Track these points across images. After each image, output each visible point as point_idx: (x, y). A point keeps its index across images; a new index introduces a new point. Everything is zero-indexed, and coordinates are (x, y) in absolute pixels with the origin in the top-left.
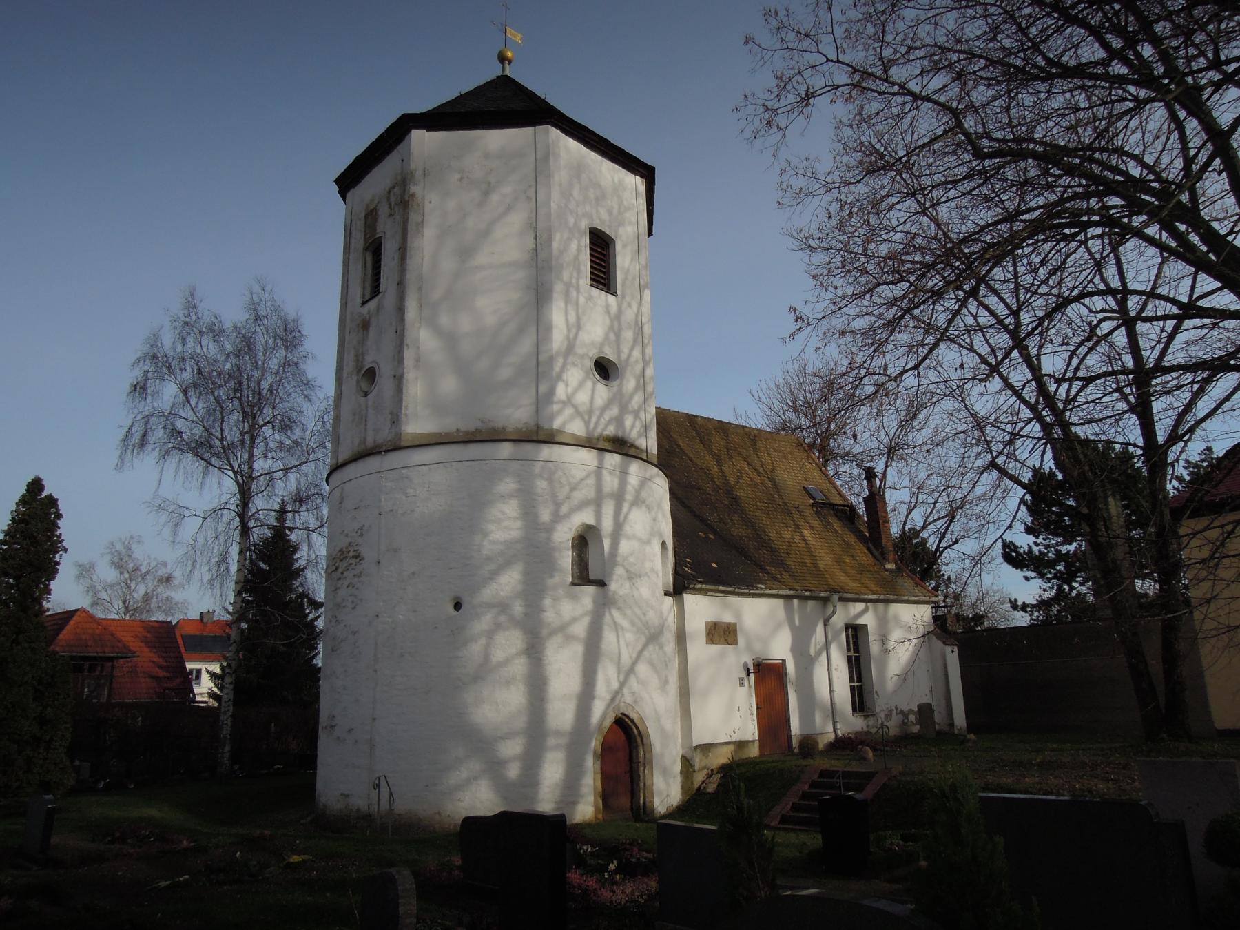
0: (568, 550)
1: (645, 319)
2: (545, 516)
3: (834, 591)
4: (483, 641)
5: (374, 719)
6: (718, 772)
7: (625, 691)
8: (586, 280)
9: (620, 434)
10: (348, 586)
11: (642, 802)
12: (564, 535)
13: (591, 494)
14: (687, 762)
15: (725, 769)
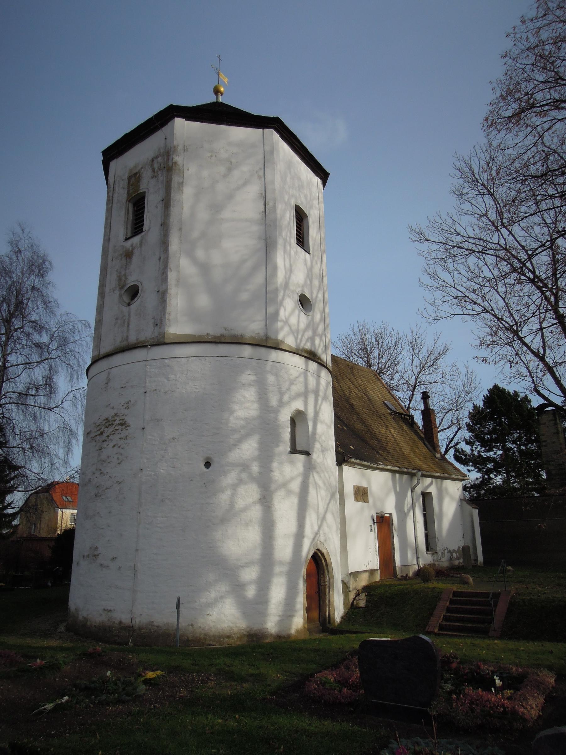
0: (288, 427)
1: (324, 274)
2: (274, 402)
3: (418, 469)
4: (229, 492)
5: (137, 550)
6: (362, 592)
7: (321, 532)
8: (294, 241)
9: (313, 350)
10: (114, 446)
11: (327, 614)
12: (285, 416)
13: (303, 389)
14: (345, 584)
15: (367, 589)
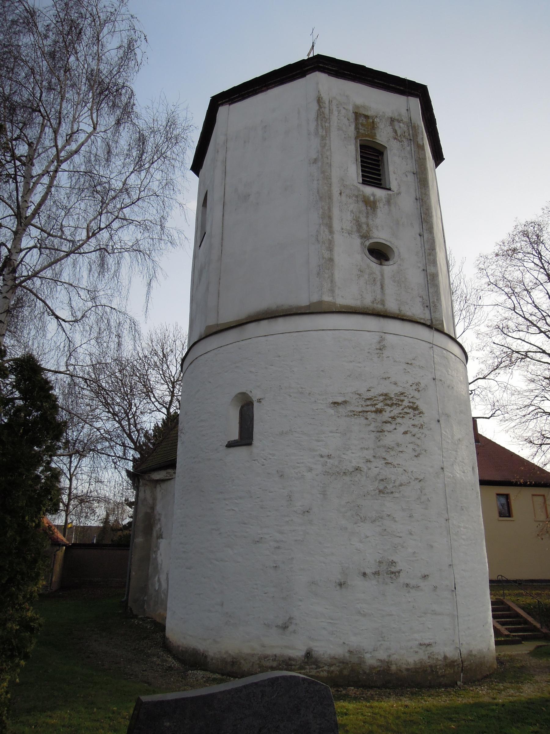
10: (405, 433)
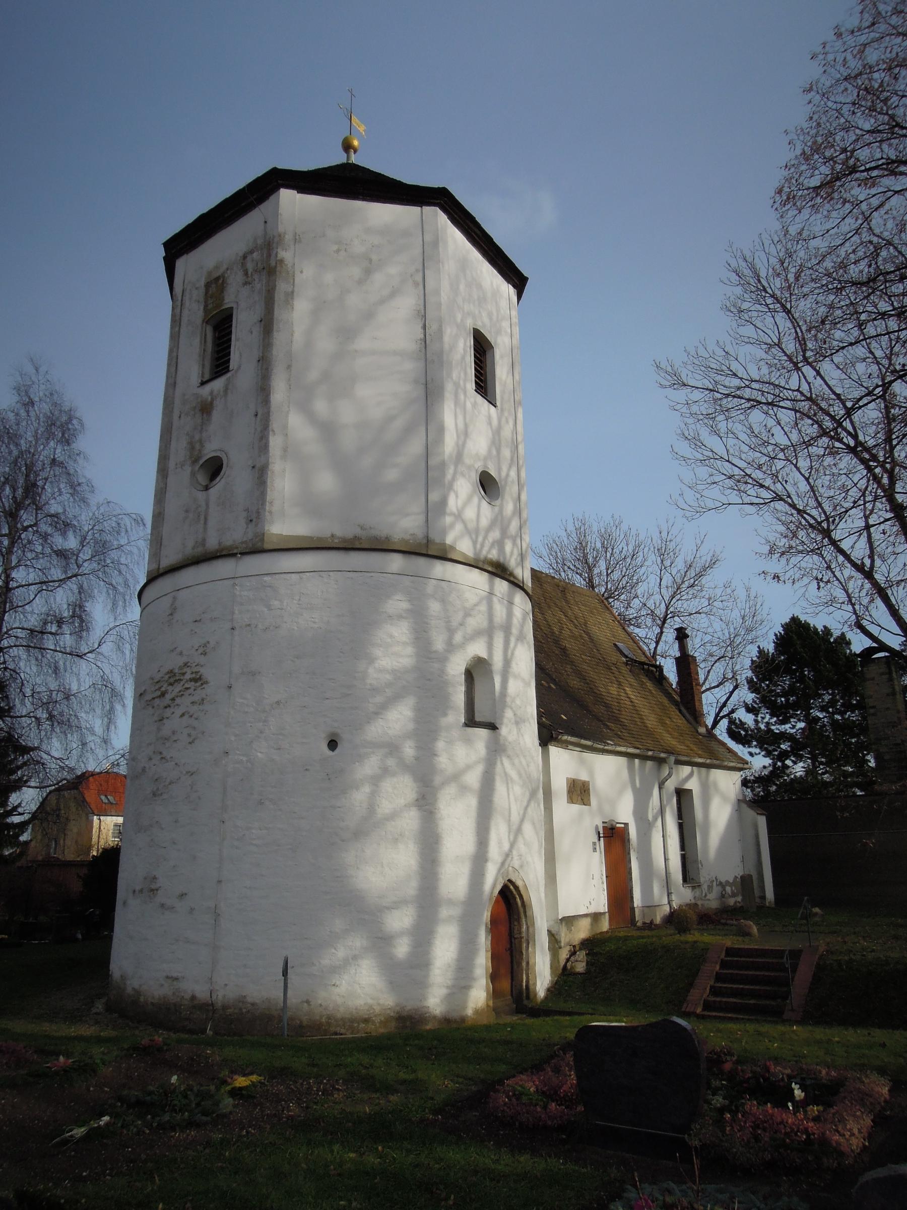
0: (461, 685)
1: (520, 438)
2: (439, 645)
3: (670, 752)
4: (367, 789)
5: (220, 882)
6: (580, 949)
7: (515, 853)
8: (471, 386)
9: (502, 560)
10: (183, 715)
11: (524, 984)
12: (457, 667)
13: (485, 624)
14: (553, 937)
15: (589, 944)
